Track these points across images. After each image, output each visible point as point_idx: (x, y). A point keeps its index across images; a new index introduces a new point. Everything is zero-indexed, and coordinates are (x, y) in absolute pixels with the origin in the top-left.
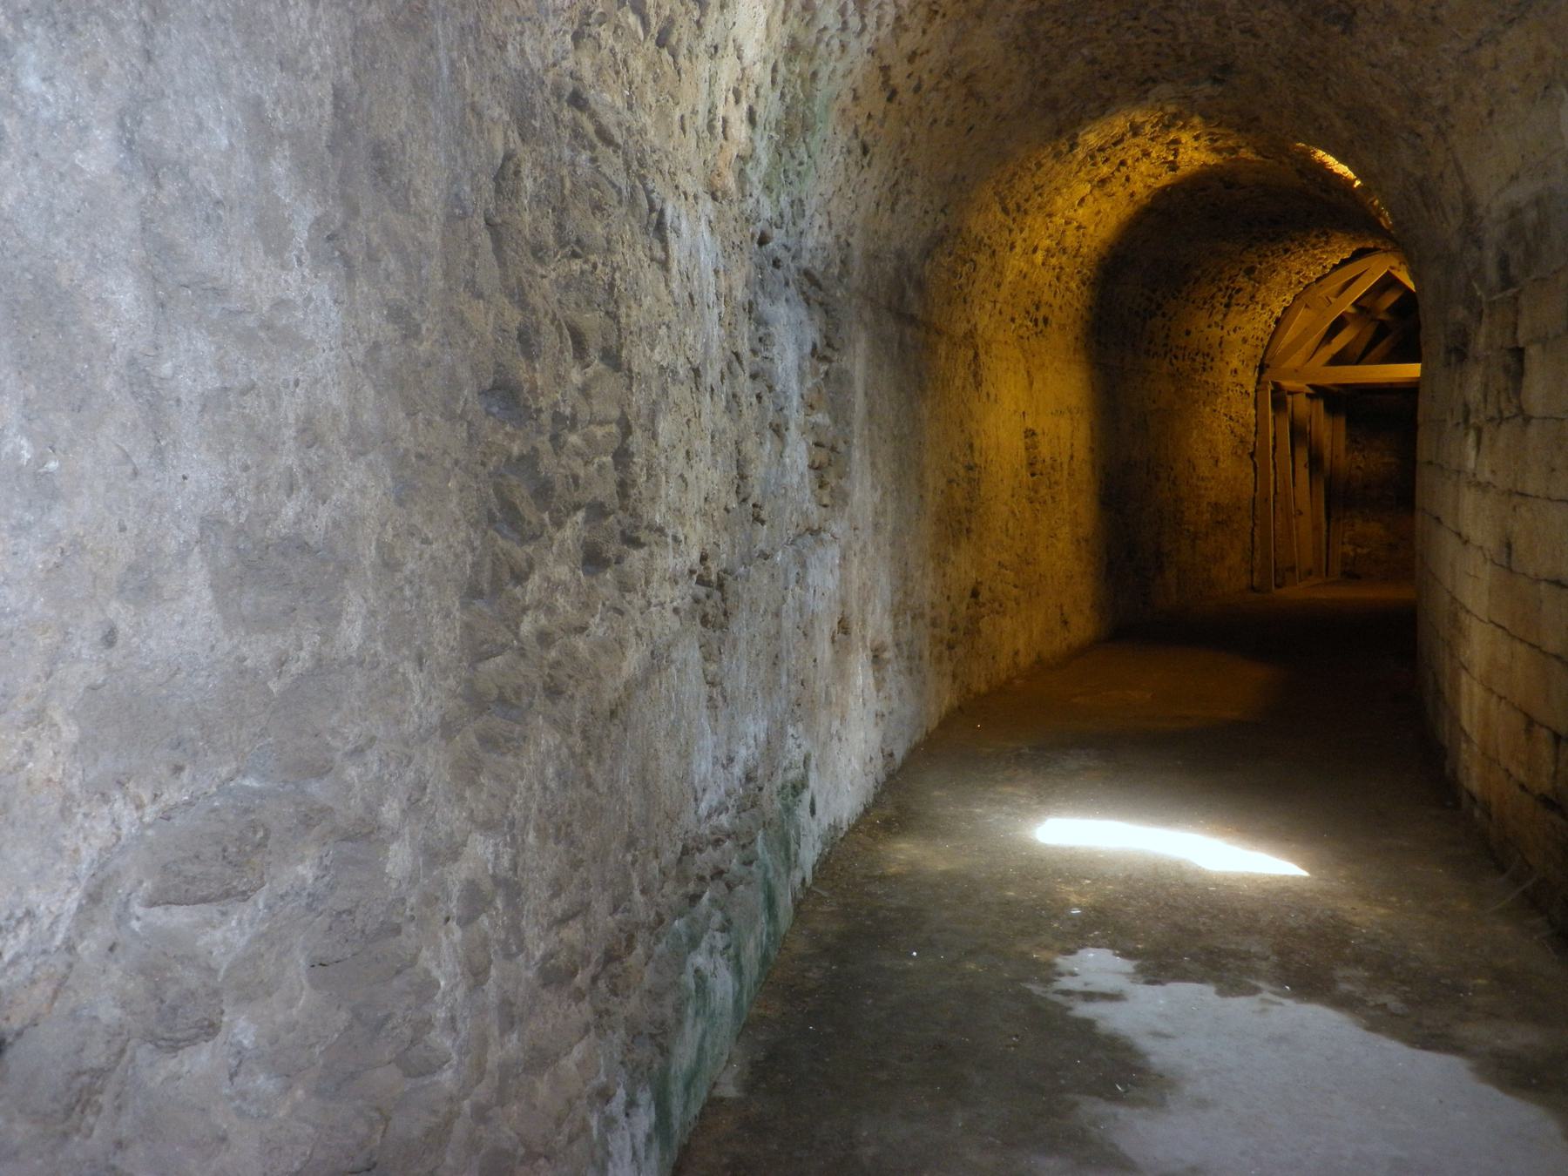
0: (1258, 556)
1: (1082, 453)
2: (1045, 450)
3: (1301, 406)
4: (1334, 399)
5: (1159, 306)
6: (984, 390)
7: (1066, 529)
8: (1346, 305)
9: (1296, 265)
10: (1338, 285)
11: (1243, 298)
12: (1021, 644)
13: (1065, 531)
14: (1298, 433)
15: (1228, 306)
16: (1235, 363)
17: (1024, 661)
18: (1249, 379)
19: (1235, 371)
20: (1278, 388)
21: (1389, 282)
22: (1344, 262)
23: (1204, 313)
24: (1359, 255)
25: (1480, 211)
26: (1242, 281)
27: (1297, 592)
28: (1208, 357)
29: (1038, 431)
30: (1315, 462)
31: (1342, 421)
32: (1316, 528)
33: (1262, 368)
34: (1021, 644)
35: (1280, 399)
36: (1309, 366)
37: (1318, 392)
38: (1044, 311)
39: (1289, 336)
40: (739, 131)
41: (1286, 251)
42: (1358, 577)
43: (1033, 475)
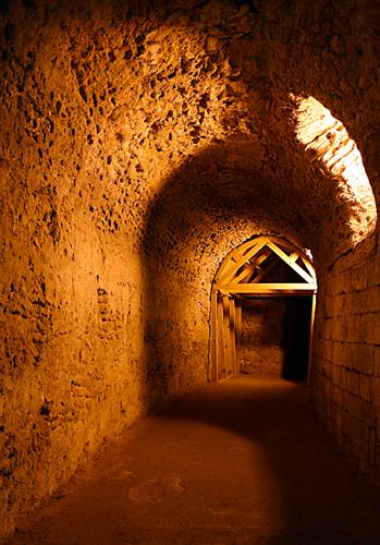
0: (211, 365)
1: (135, 311)
2: (112, 305)
3: (231, 304)
4: (240, 300)
5: (175, 243)
6: (61, 245)
7: (125, 355)
8: (246, 260)
9: (231, 237)
10: (244, 250)
11: (209, 249)
12: (90, 437)
13: (124, 357)
14: (226, 313)
15: (203, 252)
16: (203, 280)
17: (92, 448)
18: (208, 286)
19: (203, 282)
20: (219, 293)
21: (266, 249)
22: (248, 240)
23: (193, 253)
24: (254, 237)
25: (50, 453)
26: (209, 241)
27: (224, 381)
28: (192, 275)
29: (108, 292)
30: (232, 325)
31: (240, 309)
32: (233, 353)
33: (214, 282)
34: (90, 437)
35: (220, 299)
36: (234, 286)
37: (233, 297)
38: (114, 218)
39: (224, 271)
40: (10, 202)
41: (229, 228)
42: (246, 373)
43: (104, 320)
